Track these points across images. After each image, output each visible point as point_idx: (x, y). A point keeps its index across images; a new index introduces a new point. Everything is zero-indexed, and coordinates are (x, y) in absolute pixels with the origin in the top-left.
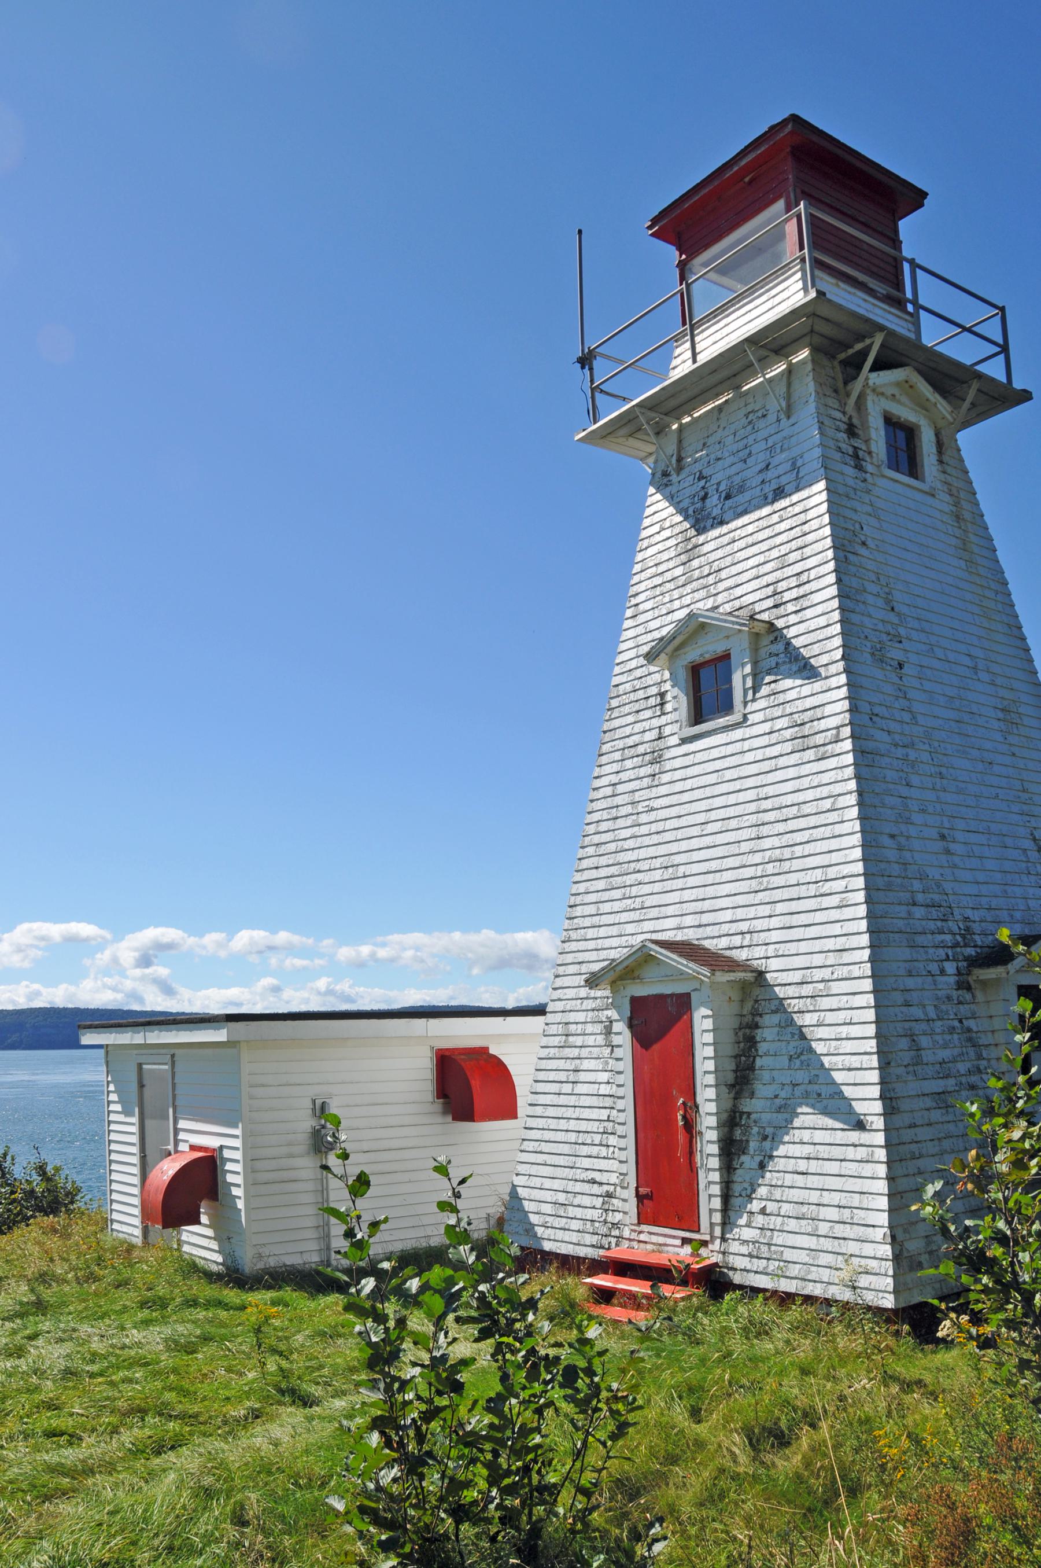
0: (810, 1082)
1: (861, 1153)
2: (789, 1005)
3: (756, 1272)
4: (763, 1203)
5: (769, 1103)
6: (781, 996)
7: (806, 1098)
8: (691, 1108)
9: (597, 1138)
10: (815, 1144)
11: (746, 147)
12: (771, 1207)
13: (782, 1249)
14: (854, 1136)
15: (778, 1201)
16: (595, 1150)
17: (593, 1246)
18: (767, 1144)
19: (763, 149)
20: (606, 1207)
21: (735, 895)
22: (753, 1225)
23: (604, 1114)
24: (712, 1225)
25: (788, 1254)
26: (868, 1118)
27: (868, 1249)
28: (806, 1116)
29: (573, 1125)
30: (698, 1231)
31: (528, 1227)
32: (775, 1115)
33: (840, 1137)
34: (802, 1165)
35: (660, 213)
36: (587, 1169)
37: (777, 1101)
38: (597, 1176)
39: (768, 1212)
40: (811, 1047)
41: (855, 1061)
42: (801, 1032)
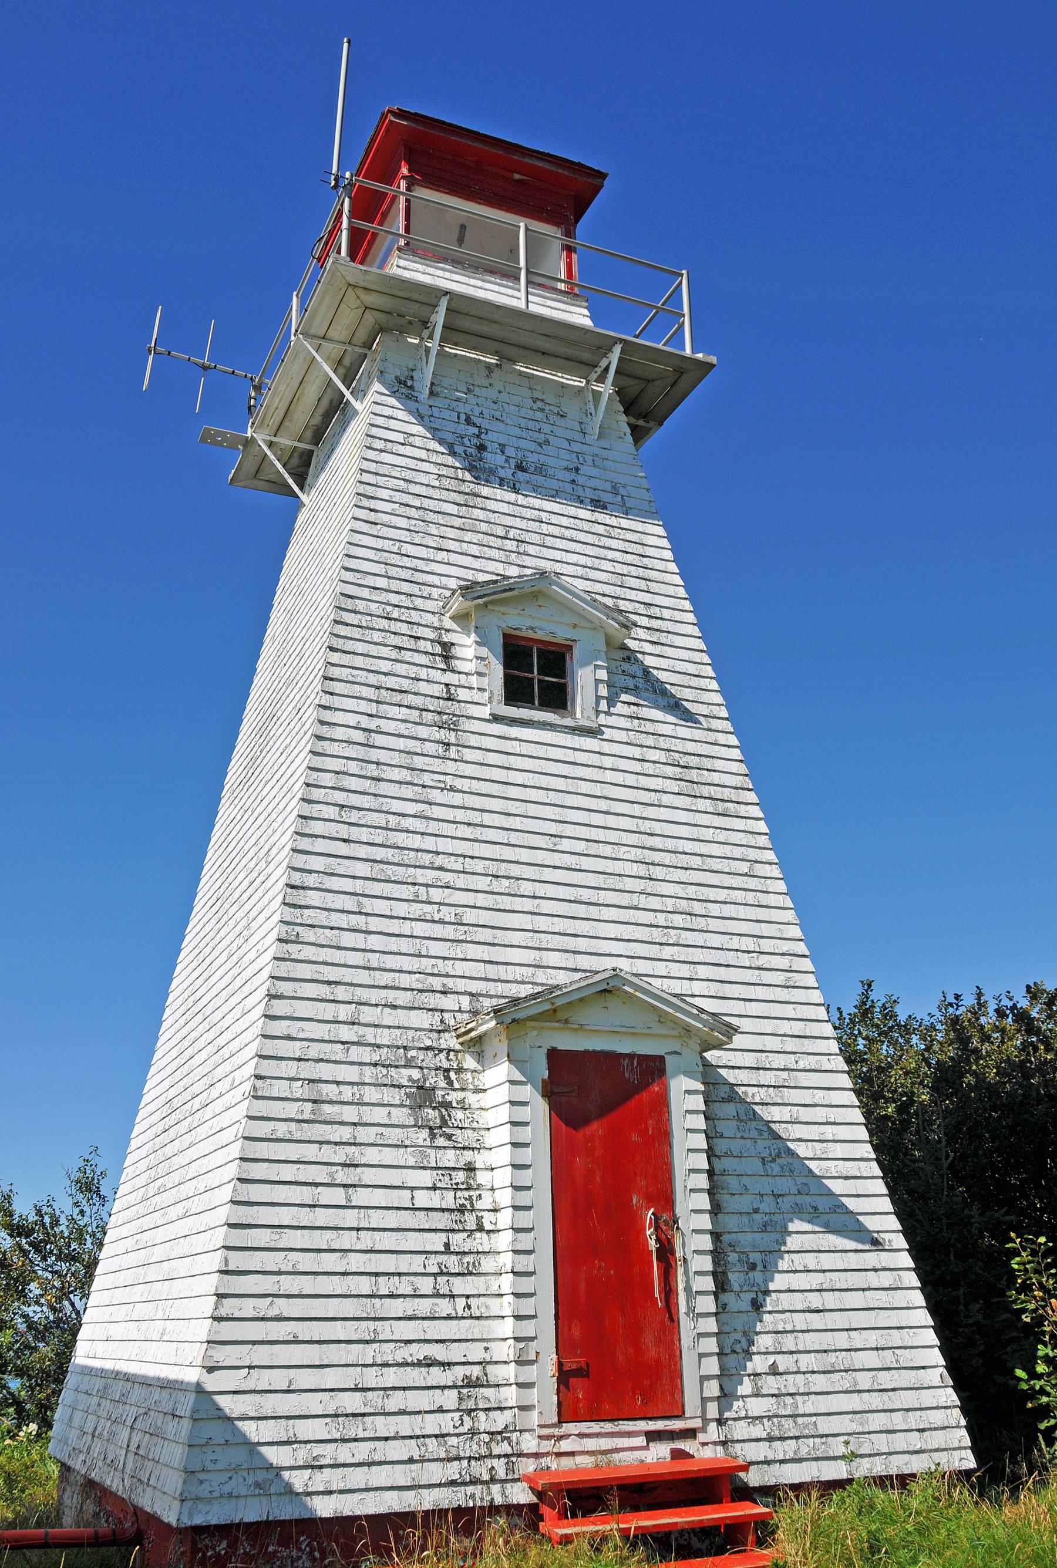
0: (800, 1193)
1: (886, 1279)
2: (745, 1093)
3: (782, 1462)
4: (771, 1359)
5: (745, 1219)
6: (732, 1081)
7: (799, 1212)
8: (666, 1223)
9: (426, 1285)
10: (824, 1271)
11: (548, 155)
12: (784, 1362)
13: (814, 1419)
14: (872, 1259)
15: (791, 1353)
16: (423, 1307)
17: (453, 1483)
18: (757, 1276)
19: (566, 173)
20: (471, 1404)
21: (629, 941)
22: (764, 1391)
23: (437, 1242)
24: (704, 1401)
25: (825, 1425)
26: (882, 1235)
27: (927, 1398)
28: (801, 1234)
29: (355, 1263)
30: (680, 1415)
31: (261, 1476)
32: (758, 1236)
33: (853, 1261)
34: (815, 1301)
35: (416, 114)
36: (408, 1342)
37: (757, 1217)
38: (438, 1352)
39: (781, 1370)
40: (789, 1149)
41: (852, 1168)
42: (770, 1128)
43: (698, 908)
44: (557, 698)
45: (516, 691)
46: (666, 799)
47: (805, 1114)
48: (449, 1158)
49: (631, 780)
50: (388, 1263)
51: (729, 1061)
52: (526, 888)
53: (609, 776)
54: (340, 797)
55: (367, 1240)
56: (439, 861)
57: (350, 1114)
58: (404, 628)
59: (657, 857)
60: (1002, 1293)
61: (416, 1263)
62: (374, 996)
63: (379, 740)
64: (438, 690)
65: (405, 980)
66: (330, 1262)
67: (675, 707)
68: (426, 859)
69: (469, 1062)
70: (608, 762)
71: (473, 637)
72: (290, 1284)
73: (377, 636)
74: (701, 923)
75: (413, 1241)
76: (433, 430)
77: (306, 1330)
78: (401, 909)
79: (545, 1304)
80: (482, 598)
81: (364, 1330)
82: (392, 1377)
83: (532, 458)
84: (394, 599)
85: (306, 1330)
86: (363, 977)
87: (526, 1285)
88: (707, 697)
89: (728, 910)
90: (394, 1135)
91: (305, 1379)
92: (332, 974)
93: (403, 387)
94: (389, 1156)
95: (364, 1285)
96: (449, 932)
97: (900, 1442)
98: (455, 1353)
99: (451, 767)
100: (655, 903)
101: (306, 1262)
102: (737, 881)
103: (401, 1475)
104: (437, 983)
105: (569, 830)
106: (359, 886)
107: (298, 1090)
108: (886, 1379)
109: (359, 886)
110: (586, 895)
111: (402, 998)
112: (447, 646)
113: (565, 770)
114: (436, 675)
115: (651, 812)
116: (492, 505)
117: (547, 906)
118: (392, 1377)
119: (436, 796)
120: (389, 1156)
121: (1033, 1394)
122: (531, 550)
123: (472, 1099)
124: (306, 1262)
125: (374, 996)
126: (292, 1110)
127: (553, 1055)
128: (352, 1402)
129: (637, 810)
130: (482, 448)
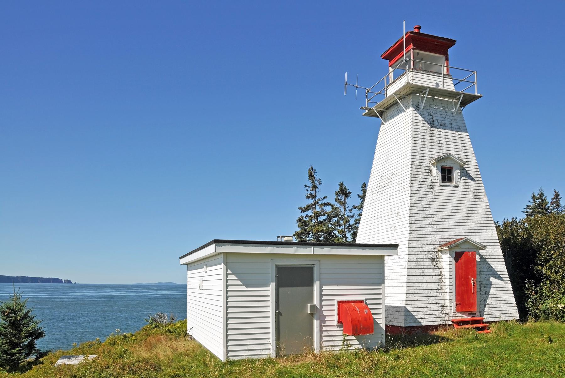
1: (507, 289)
9: (435, 291)
16: (435, 294)
23: (436, 284)
25: (496, 312)
27: (512, 308)
29: (425, 288)
38: (438, 301)
43: (476, 222)
44: (450, 179)
45: (443, 180)
46: (471, 200)
47: (494, 260)
48: (438, 270)
49: (464, 196)
50: (429, 288)
51: (483, 252)
52: (447, 220)
53: (460, 196)
54: (416, 205)
55: (426, 284)
56: (433, 216)
57: (422, 263)
58: (423, 167)
59: (469, 212)
60: (523, 290)
61: (434, 288)
62: (425, 243)
63: (421, 192)
64: (430, 181)
65: (429, 239)
66: (421, 288)
67: (472, 179)
68: (430, 216)
69: (440, 254)
70: (460, 193)
71: (436, 168)
72: (416, 292)
73: (419, 170)
74: (477, 225)
75: (433, 284)
76: (424, 118)
77: (419, 299)
78: (427, 226)
79: (454, 294)
80: (439, 160)
81: (427, 298)
82: (431, 305)
83: (443, 122)
84: (421, 161)
85: (419, 299)
86: (422, 239)
87: (451, 291)
88: (477, 176)
89: (482, 222)
90: (429, 267)
91: (419, 306)
92: (418, 239)
93: (417, 108)
94: (429, 270)
95: (426, 291)
96: (435, 230)
97: (507, 315)
98: (440, 302)
99: (433, 197)
100: (469, 221)
101: (418, 288)
102: (483, 216)
103: (434, 320)
104: (434, 239)
105: (454, 208)
106: (420, 222)
107: (414, 260)
108: (506, 305)
109: (420, 222)
110: (457, 221)
111: (429, 243)
112: (431, 170)
113: (453, 195)
114: (429, 177)
115: (468, 203)
116: (437, 136)
117: (451, 224)
118: (431, 305)
119: (431, 203)
120: (429, 270)
121: (527, 308)
122: (444, 145)
123: (440, 260)
124: (418, 288)
125: (425, 243)
126: (414, 263)
127: (456, 253)
128: (426, 309)
129: (465, 202)
130: (433, 121)
